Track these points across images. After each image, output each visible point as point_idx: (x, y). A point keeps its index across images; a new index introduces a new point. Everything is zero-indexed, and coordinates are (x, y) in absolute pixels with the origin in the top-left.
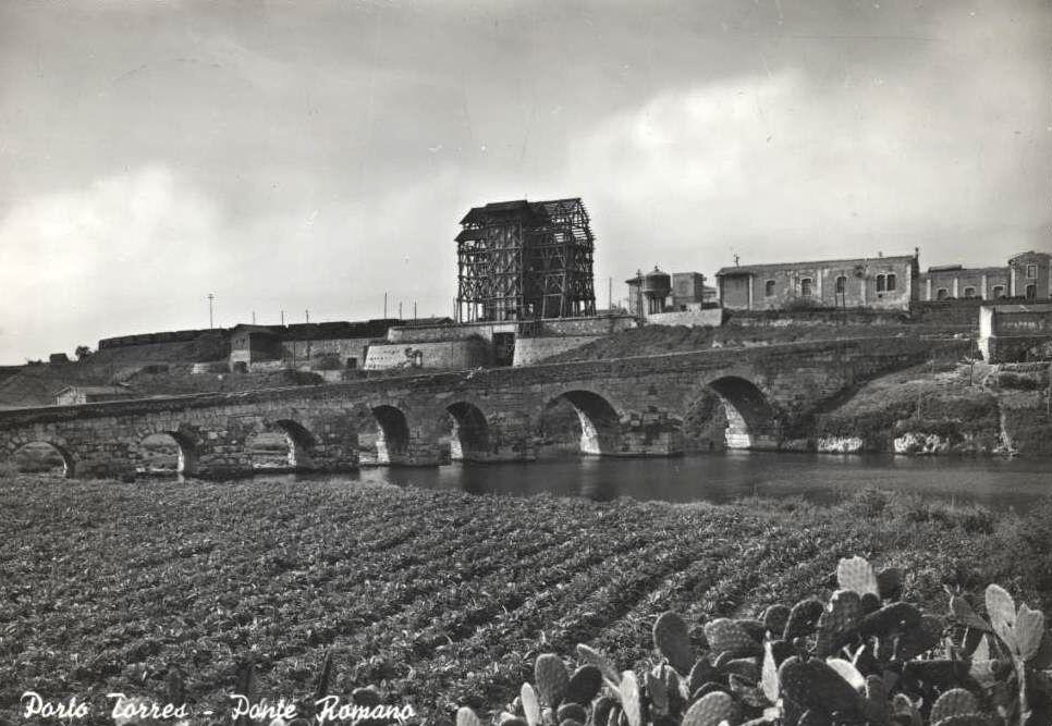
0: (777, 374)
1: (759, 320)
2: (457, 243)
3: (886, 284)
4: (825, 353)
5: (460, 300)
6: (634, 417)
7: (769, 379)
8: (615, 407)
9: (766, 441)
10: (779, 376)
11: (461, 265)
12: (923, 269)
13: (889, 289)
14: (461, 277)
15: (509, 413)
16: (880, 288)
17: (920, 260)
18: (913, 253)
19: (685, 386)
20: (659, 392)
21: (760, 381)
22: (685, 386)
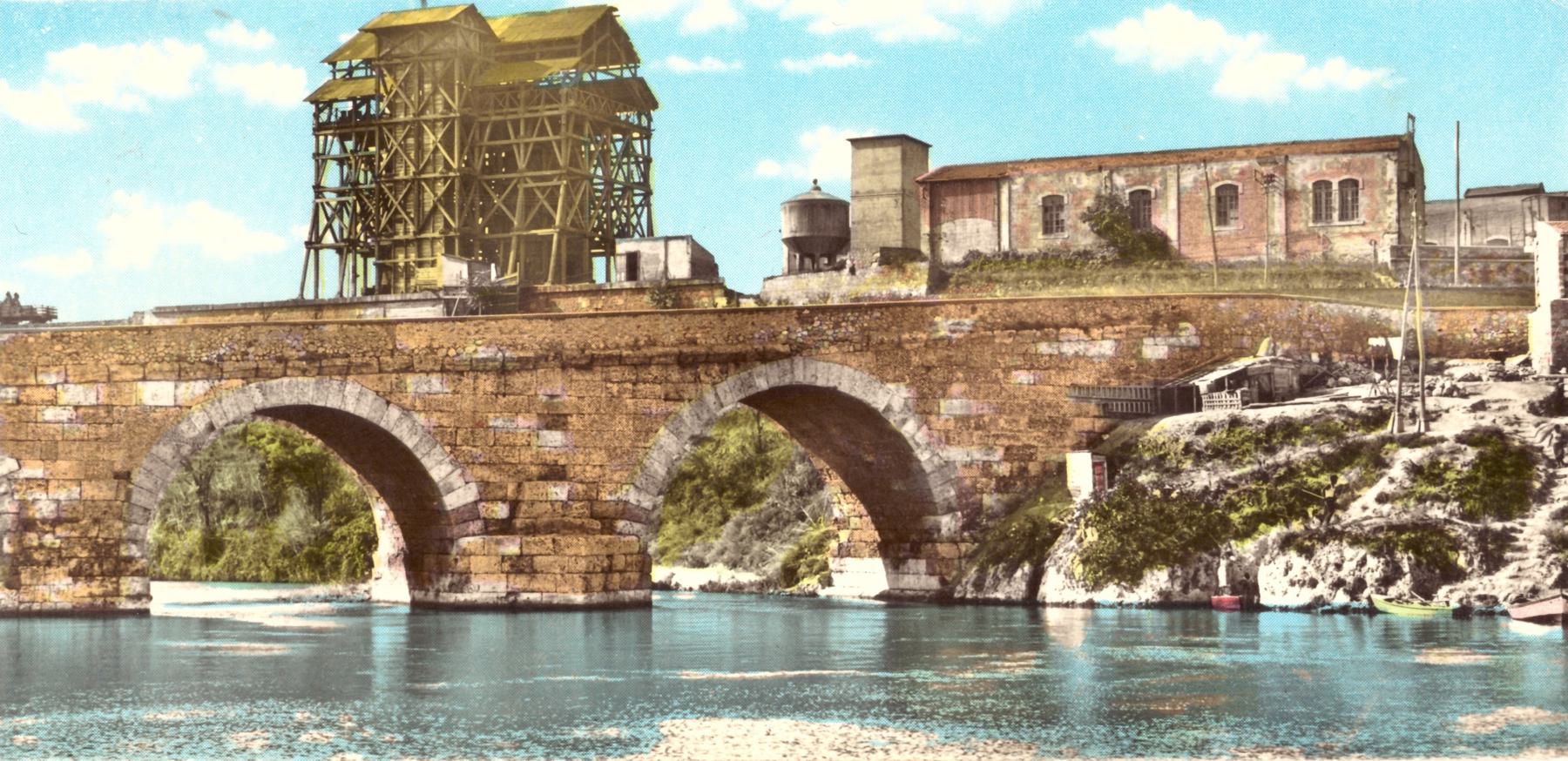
0: (949, 382)
1: (1271, 451)
2: (312, 108)
3: (1336, 204)
4: (1095, 332)
5: (314, 244)
6: (487, 492)
7: (922, 397)
8: (427, 462)
9: (918, 578)
10: (956, 388)
11: (320, 159)
12: (1438, 186)
13: (1343, 216)
14: (318, 190)
15: (62, 465)
16: (1321, 212)
17: (1421, 144)
18: (1399, 129)
19: (656, 407)
20: (573, 420)
21: (897, 404)
22: (656, 407)
